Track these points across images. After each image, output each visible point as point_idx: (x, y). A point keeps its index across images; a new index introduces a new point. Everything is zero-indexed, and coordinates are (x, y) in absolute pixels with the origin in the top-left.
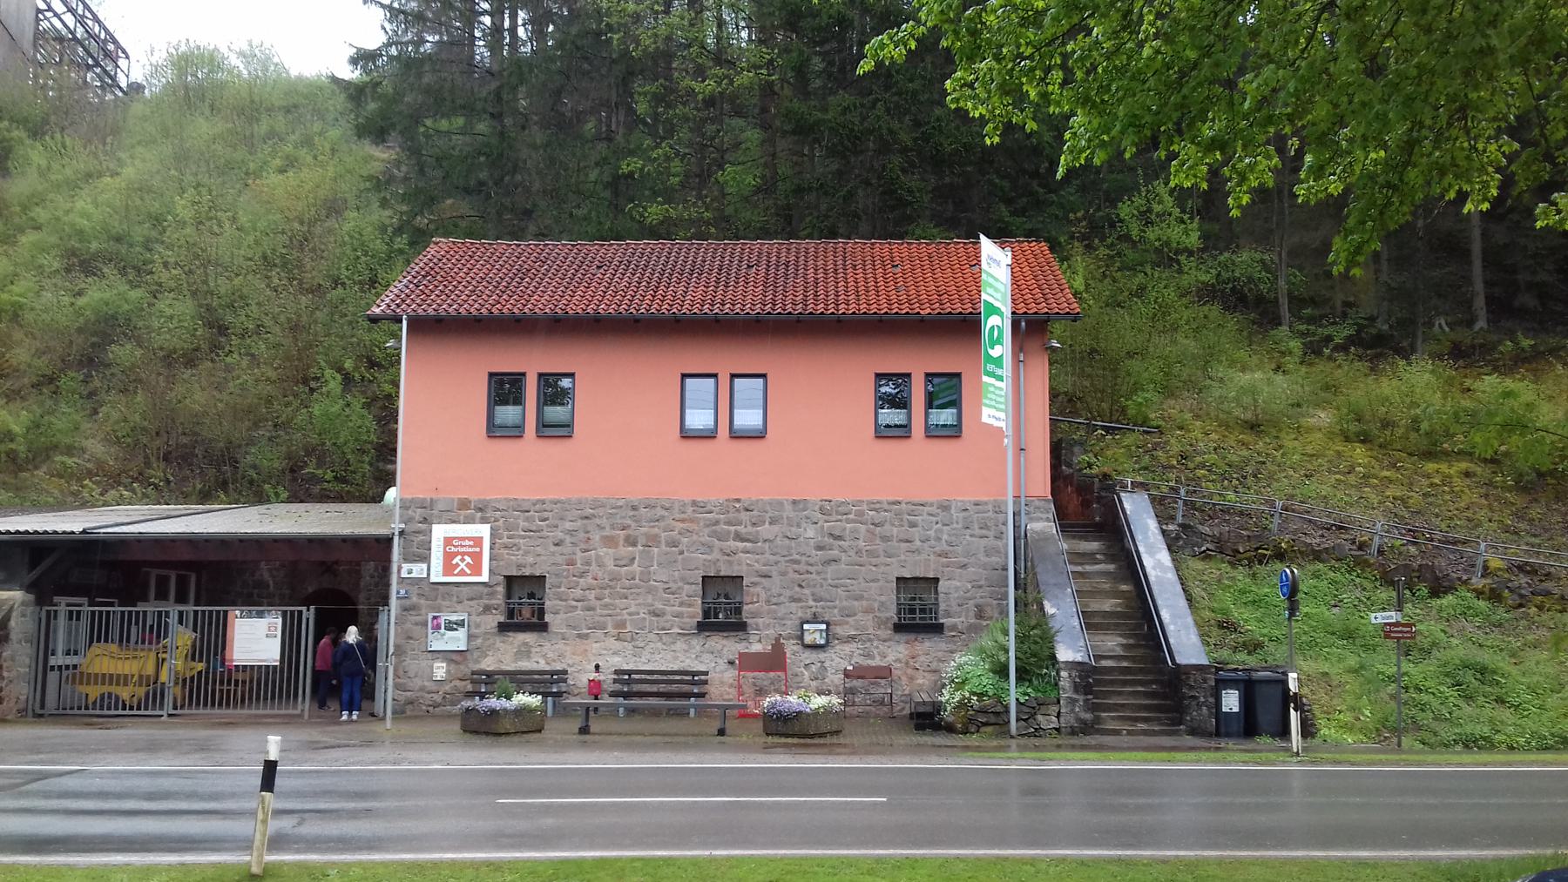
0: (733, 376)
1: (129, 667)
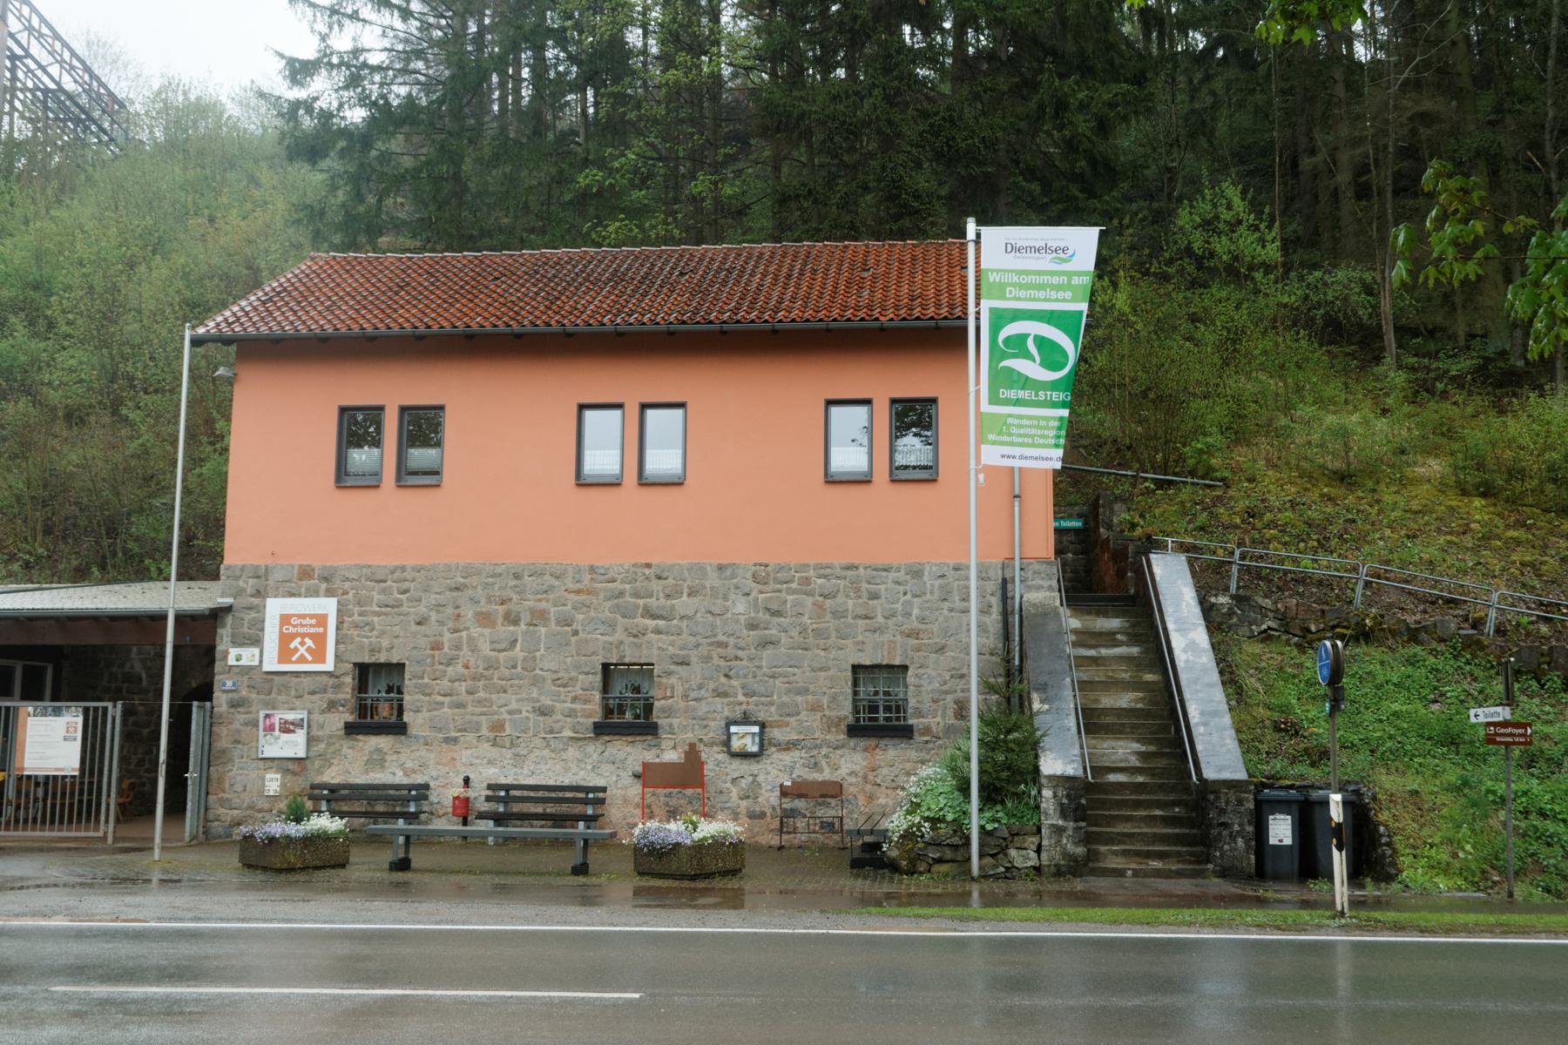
0: (644, 407)
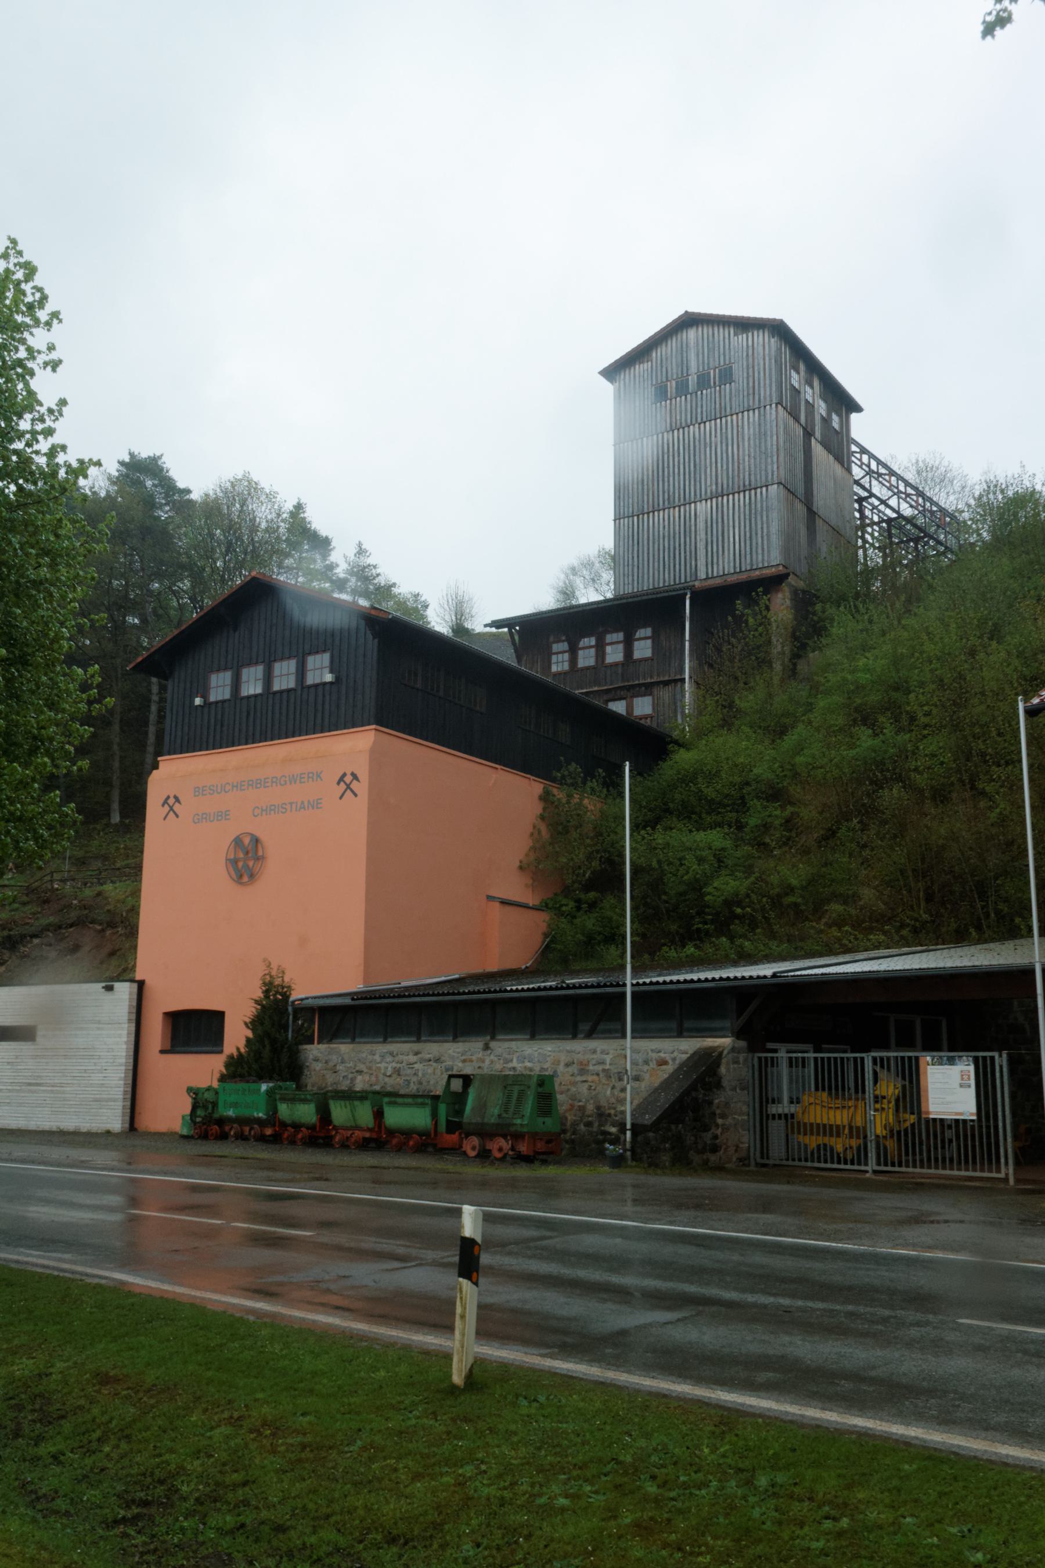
1: (839, 1118)
